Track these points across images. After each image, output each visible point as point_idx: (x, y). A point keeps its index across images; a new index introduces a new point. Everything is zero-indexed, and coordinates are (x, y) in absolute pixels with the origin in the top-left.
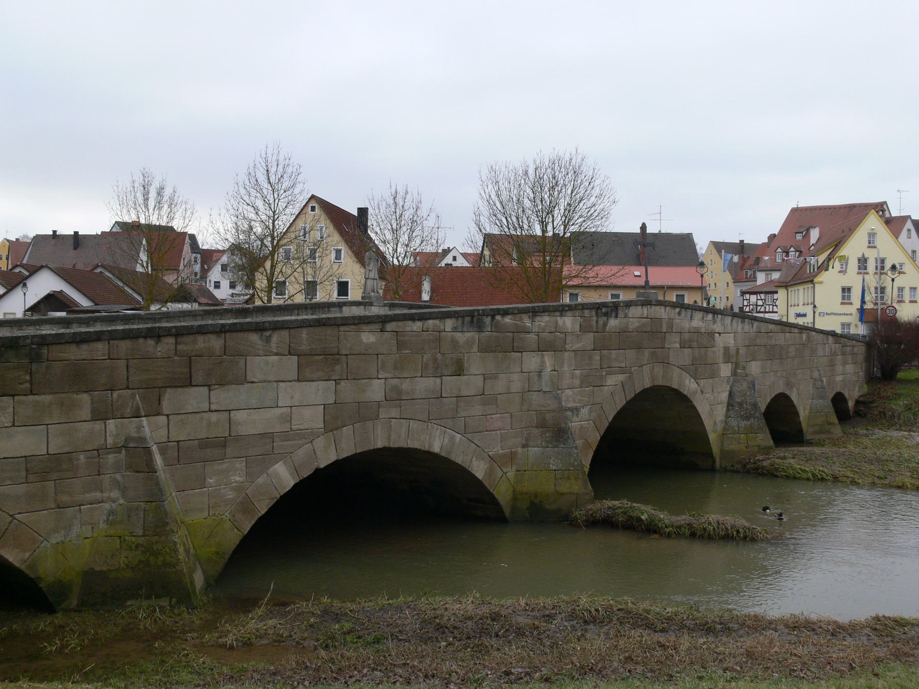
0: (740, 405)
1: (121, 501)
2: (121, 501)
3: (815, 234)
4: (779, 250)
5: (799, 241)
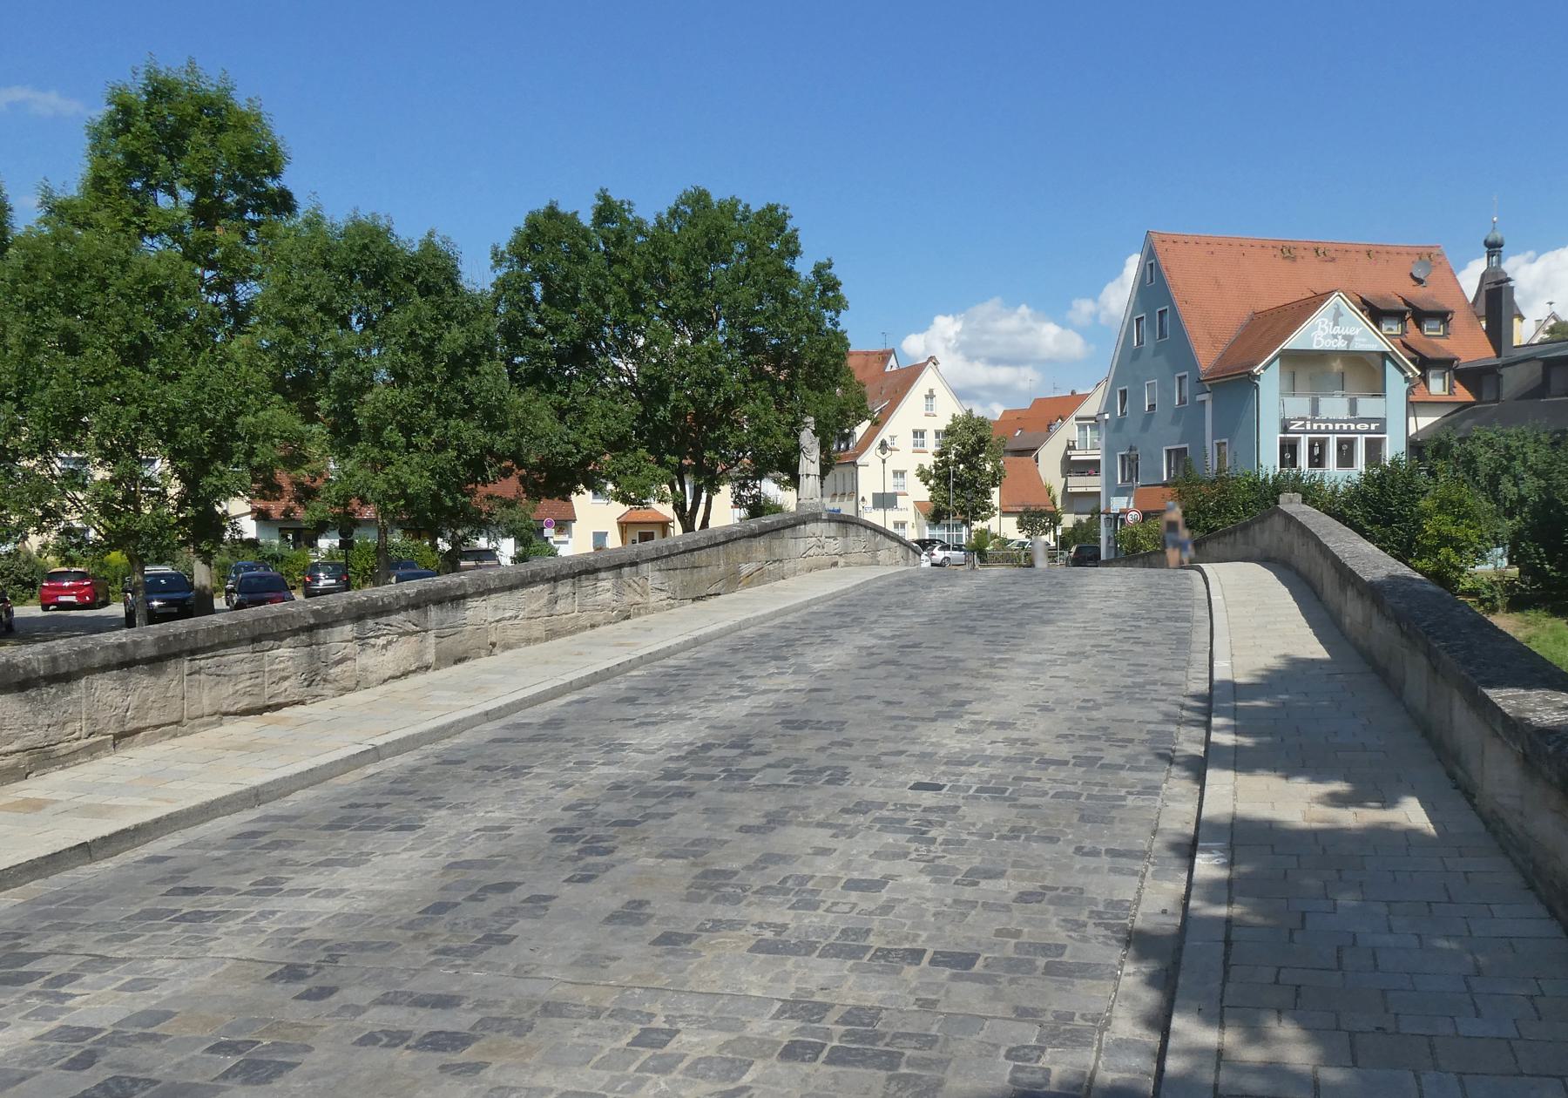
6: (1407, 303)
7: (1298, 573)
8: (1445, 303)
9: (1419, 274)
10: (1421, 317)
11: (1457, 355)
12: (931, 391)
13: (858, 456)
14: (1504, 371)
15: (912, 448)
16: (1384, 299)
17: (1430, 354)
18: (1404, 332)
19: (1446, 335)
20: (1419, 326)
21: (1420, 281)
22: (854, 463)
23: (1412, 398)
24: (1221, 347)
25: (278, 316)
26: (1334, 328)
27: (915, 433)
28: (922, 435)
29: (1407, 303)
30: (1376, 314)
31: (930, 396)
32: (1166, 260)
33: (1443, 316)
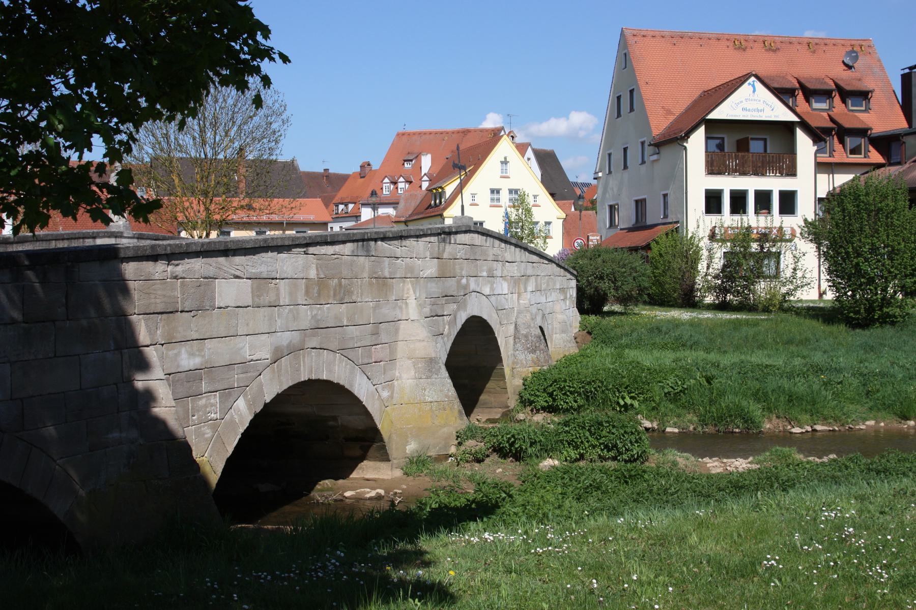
0: (526, 336)
1: (141, 441)
2: (141, 441)
3: (426, 162)
4: (386, 180)
5: (408, 170)
6: (799, 82)
7: (491, 236)
8: (867, 84)
9: (847, 61)
10: (846, 95)
11: (871, 125)
12: (505, 158)
13: (445, 209)
14: (905, 139)
15: (489, 203)
16: (820, 80)
17: (847, 124)
18: (831, 107)
19: (867, 110)
20: (808, 101)
21: (850, 67)
22: (441, 215)
23: (819, 160)
24: (672, 118)
25: (834, 237)
26: (753, 103)
27: (492, 191)
28: (498, 192)
29: (836, 85)
30: (783, 93)
31: (505, 162)
32: (636, 51)
33: (864, 95)
